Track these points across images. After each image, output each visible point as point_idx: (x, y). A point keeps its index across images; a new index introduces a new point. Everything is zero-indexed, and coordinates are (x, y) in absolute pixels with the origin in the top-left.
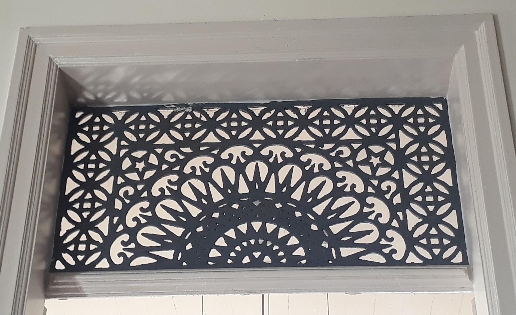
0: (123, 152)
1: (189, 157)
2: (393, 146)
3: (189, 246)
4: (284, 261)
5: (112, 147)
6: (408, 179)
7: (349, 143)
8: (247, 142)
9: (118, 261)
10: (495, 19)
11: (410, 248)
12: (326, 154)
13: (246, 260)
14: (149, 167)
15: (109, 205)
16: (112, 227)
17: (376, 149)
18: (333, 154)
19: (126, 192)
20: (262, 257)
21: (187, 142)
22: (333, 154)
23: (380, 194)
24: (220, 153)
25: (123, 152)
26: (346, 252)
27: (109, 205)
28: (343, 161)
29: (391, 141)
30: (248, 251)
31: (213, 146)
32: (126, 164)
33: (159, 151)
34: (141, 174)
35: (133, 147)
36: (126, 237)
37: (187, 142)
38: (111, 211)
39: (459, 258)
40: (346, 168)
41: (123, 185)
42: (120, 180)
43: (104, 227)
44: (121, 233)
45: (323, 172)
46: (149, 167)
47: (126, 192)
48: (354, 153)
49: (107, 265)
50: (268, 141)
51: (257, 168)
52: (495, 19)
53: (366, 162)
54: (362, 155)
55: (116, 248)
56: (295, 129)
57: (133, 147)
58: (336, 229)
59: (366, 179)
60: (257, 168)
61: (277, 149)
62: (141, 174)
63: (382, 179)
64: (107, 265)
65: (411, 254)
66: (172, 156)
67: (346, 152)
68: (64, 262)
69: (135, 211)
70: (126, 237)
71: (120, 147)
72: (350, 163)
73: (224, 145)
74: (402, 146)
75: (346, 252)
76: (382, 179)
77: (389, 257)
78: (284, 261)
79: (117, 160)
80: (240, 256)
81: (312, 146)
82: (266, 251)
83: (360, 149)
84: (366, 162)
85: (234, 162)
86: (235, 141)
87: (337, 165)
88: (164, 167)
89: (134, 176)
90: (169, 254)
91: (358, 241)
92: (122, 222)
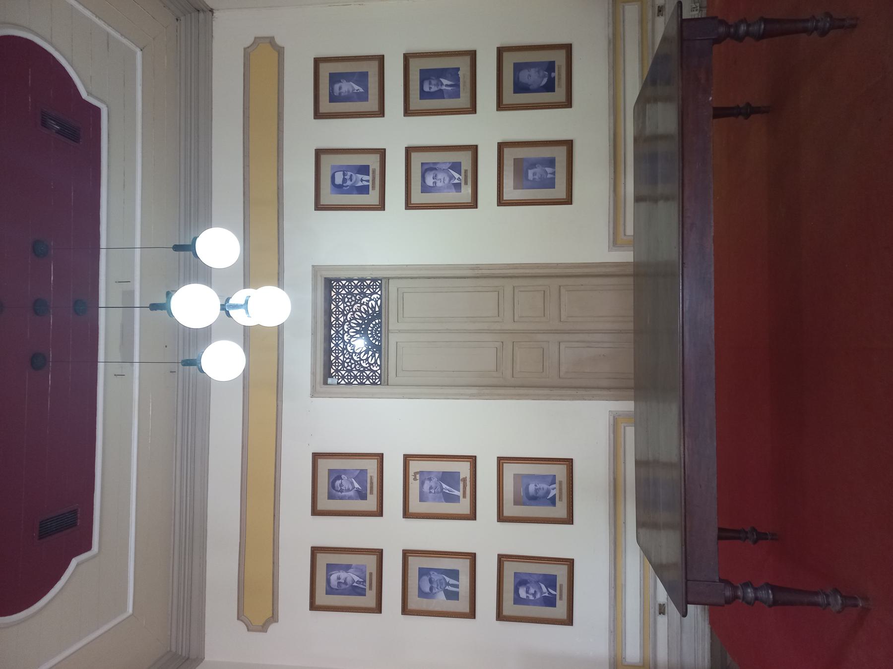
0: (345, 369)
1: (347, 351)
2: (345, 295)
3: (375, 315)
4: (380, 320)
5: (343, 372)
6: (342, 358)
7: (344, 307)
8: (343, 335)
9: (378, 368)
10: (171, 372)
11: (377, 293)
12: (348, 314)
13: (379, 335)
14: (350, 362)
15: (362, 372)
16: (368, 370)
17: (346, 300)
18: (348, 312)
19: (358, 367)
20: (378, 331)
21: (342, 351)
22: (348, 312)
23: (361, 300)
24: (346, 342)
25: (345, 369)
26: (377, 309)
27: (362, 372)
28: (350, 309)
29: (344, 296)
30: (377, 335)
31: (344, 345)
32: (349, 368)
33: (345, 359)
34: (353, 364)
35: (344, 367)
36: (372, 366)
37: (342, 351)
38: (364, 371)
39: (380, 282)
40: (352, 308)
41: (356, 368)
42: (354, 369)
43: (368, 372)
44: (371, 368)
45: (353, 315)
46: (350, 362)
47: (358, 367)
48: (347, 306)
49: (379, 371)
50: (343, 329)
51: (357, 314)
52: (171, 372)
53: (350, 303)
54: (348, 304)
55: (375, 369)
56: (339, 321)
57: (344, 367)
58: (370, 312)
59: (356, 303)
60: (357, 314)
61: (346, 327)
62: (353, 364)
63: (356, 299)
64: (379, 371)
65: (378, 293)
66: (359, 297)
67: (347, 308)
68: (379, 283)
69: (364, 365)
70: (372, 366)
71: (344, 370)
72: (350, 307)
73: (344, 341)
74: (345, 293)
75: (377, 309)
76: (356, 299)
77: (379, 299)
78: (380, 320)
79: (347, 371)
80: (379, 337)
81: (345, 317)
82: (376, 330)
83: (346, 304)
84: (350, 303)
85: (349, 339)
86: (343, 338)
87: (351, 310)
88: (350, 357)
89: (353, 366)
90: (377, 355)
91: (374, 306)
92: (367, 368)
